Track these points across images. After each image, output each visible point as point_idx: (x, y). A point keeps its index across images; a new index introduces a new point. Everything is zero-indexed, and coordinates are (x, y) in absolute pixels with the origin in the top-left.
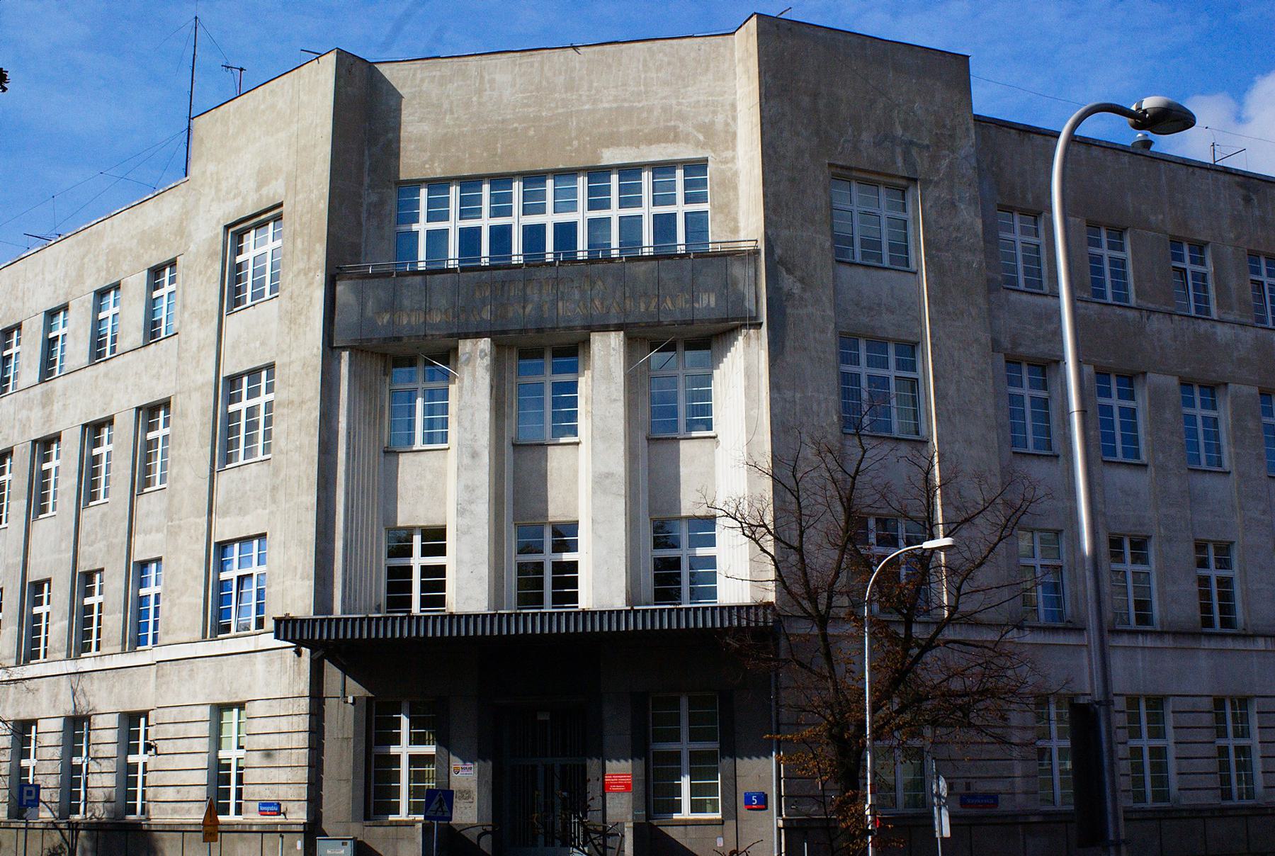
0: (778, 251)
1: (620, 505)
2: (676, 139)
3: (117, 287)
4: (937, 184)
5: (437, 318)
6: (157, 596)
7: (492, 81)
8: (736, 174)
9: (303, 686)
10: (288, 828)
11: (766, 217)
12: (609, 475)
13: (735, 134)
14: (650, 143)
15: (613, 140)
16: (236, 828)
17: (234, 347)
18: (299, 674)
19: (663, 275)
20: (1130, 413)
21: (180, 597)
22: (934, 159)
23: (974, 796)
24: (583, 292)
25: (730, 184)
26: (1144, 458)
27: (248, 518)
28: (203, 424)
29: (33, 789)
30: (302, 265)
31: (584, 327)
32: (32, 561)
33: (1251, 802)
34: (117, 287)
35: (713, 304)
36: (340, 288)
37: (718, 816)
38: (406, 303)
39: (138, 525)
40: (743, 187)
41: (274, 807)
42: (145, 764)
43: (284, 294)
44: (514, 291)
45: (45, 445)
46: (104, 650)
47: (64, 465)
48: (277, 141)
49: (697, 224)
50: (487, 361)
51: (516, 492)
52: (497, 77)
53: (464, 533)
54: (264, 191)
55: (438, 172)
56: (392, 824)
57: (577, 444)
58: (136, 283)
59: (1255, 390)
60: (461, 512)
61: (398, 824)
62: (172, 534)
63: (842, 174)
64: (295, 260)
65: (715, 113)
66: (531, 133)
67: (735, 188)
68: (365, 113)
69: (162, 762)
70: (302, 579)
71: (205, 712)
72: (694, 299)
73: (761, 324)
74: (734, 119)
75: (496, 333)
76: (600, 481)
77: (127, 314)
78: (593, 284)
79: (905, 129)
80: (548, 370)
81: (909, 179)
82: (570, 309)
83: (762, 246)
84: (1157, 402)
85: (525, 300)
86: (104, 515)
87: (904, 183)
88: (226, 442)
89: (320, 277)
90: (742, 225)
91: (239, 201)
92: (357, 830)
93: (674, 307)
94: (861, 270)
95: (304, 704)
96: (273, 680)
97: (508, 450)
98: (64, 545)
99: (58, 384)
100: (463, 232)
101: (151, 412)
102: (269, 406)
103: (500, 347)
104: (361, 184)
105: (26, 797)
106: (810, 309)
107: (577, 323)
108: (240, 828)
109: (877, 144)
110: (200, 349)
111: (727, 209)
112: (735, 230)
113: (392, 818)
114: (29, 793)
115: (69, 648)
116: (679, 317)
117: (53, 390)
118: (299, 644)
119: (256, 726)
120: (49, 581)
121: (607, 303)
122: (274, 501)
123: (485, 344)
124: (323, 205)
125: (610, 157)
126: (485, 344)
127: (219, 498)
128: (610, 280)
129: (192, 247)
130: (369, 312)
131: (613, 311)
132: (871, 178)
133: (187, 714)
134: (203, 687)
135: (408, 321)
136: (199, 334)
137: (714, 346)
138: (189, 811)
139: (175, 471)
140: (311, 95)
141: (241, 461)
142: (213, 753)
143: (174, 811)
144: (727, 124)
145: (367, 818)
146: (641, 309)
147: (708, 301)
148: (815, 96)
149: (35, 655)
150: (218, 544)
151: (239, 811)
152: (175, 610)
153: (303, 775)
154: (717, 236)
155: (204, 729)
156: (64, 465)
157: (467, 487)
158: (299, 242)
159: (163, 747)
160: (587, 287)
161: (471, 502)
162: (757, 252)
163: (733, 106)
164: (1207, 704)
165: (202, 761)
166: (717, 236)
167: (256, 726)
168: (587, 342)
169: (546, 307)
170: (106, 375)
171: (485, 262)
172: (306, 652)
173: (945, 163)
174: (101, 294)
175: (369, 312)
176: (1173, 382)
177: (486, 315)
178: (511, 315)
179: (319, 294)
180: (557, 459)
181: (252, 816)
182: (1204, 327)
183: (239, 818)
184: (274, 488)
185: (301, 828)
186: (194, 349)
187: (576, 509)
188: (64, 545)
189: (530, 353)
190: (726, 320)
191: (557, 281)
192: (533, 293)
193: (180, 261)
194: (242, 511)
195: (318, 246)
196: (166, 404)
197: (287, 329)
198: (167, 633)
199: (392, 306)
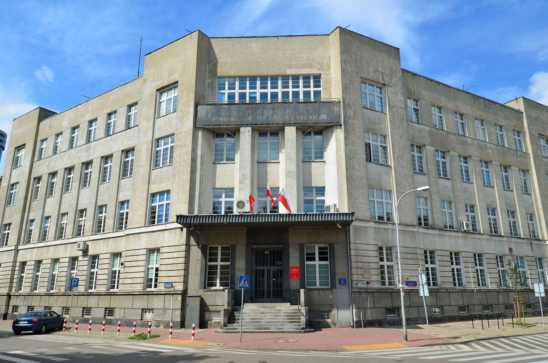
0: (346, 102)
1: (295, 182)
2: (311, 67)
3: (115, 112)
4: (391, 87)
5: (233, 119)
6: (127, 214)
7: (250, 46)
8: (330, 78)
9: (184, 241)
10: (176, 292)
11: (343, 91)
12: (291, 171)
13: (330, 66)
14: (302, 68)
15: (290, 67)
16: (154, 293)
17: (159, 129)
18: (182, 236)
19: (309, 108)
20: (444, 163)
21: (137, 214)
22: (391, 79)
23: (410, 282)
24: (282, 113)
25: (329, 82)
26: (449, 177)
27: (163, 185)
28: (147, 154)
29: (76, 280)
30: (185, 101)
31: (283, 124)
32: (80, 203)
33: (484, 288)
34: (115, 112)
35: (325, 118)
36: (199, 108)
37: (329, 287)
38: (222, 114)
39: (120, 189)
40: (333, 82)
41: (170, 285)
42: (119, 271)
43: (178, 112)
44: (259, 112)
45: (87, 164)
46: (105, 232)
47: (94, 171)
48: (179, 61)
49: (317, 94)
50: (250, 133)
51: (258, 177)
52: (252, 44)
53: (242, 190)
54: (171, 77)
55: (232, 73)
56: (214, 291)
57: (279, 162)
58: (122, 111)
59: (479, 159)
60: (241, 183)
61: (216, 291)
62: (135, 191)
63: (364, 81)
64: (186, 95)
65: (324, 59)
66: (263, 63)
67: (330, 83)
68: (206, 58)
69: (127, 270)
70: (184, 204)
71: (144, 252)
72: (319, 116)
73: (341, 125)
74: (330, 61)
75: (253, 125)
76: (288, 174)
77: (119, 121)
78: (286, 110)
79: (382, 69)
80: (269, 139)
81: (383, 84)
82: (277, 118)
83: (341, 100)
84: (451, 161)
85: (263, 114)
86: (108, 186)
87: (382, 85)
88: (155, 161)
89: (192, 104)
90: (333, 95)
91: (162, 81)
92: (201, 292)
93: (312, 119)
94: (370, 111)
95: (183, 248)
96: (173, 238)
97: (256, 163)
98: (92, 197)
99: (92, 144)
100: (240, 94)
101: (127, 152)
102: (172, 148)
103: (253, 130)
104: (206, 76)
105: (73, 283)
106: (356, 121)
107: (281, 122)
108: (156, 293)
109: (374, 72)
110: (146, 130)
111: (328, 89)
112: (331, 96)
113: (213, 288)
114: (75, 282)
115: (92, 231)
116: (314, 122)
117: (90, 146)
118: (185, 225)
119: (164, 256)
120: (86, 209)
121: (290, 116)
122: (173, 178)
123: (249, 129)
124: (194, 81)
125: (290, 72)
126: (249, 129)
127: (152, 178)
128: (291, 109)
129: (144, 97)
130: (209, 116)
131: (292, 119)
132: (372, 83)
133: (137, 252)
134: (145, 242)
135: (223, 120)
136: (145, 124)
137: (324, 133)
138: (136, 287)
139: (136, 170)
140: (189, 48)
141: (161, 166)
142: (146, 266)
143: (130, 287)
144: (328, 63)
145: (205, 288)
146: (302, 119)
147: (324, 117)
148: (356, 55)
149: (79, 235)
150: (151, 194)
151: (156, 286)
152: (134, 217)
153: (182, 273)
154: (324, 97)
155: (144, 258)
156: (94, 171)
157: (243, 174)
158: (184, 93)
159: (126, 264)
160: (284, 111)
161: (244, 179)
162: (340, 102)
163: (330, 57)
164: (472, 255)
165: (142, 269)
166: (324, 97)
167: (164, 256)
168: (283, 129)
169: (270, 117)
170: (111, 140)
171: (248, 102)
172: (185, 230)
173: (394, 80)
174: (110, 115)
175: (209, 116)
176: (457, 154)
177: (250, 119)
178: (258, 119)
179: (192, 109)
180: (271, 167)
181: (161, 288)
182: (464, 138)
183: (156, 289)
184: (174, 174)
185: (181, 292)
186: (144, 130)
187: (278, 183)
188: (92, 197)
189: (262, 134)
190: (329, 123)
191: (274, 109)
192: (266, 113)
193: (139, 102)
194: (161, 182)
195: (191, 94)
196: (133, 149)
197: (179, 121)
198: (131, 225)
199: (218, 116)
